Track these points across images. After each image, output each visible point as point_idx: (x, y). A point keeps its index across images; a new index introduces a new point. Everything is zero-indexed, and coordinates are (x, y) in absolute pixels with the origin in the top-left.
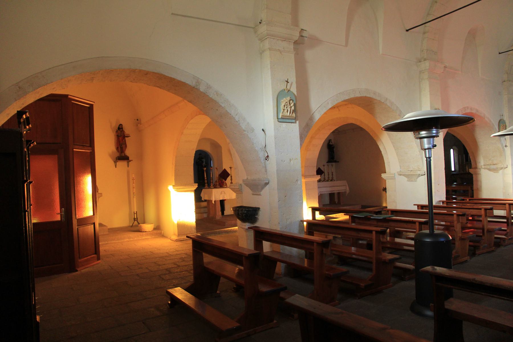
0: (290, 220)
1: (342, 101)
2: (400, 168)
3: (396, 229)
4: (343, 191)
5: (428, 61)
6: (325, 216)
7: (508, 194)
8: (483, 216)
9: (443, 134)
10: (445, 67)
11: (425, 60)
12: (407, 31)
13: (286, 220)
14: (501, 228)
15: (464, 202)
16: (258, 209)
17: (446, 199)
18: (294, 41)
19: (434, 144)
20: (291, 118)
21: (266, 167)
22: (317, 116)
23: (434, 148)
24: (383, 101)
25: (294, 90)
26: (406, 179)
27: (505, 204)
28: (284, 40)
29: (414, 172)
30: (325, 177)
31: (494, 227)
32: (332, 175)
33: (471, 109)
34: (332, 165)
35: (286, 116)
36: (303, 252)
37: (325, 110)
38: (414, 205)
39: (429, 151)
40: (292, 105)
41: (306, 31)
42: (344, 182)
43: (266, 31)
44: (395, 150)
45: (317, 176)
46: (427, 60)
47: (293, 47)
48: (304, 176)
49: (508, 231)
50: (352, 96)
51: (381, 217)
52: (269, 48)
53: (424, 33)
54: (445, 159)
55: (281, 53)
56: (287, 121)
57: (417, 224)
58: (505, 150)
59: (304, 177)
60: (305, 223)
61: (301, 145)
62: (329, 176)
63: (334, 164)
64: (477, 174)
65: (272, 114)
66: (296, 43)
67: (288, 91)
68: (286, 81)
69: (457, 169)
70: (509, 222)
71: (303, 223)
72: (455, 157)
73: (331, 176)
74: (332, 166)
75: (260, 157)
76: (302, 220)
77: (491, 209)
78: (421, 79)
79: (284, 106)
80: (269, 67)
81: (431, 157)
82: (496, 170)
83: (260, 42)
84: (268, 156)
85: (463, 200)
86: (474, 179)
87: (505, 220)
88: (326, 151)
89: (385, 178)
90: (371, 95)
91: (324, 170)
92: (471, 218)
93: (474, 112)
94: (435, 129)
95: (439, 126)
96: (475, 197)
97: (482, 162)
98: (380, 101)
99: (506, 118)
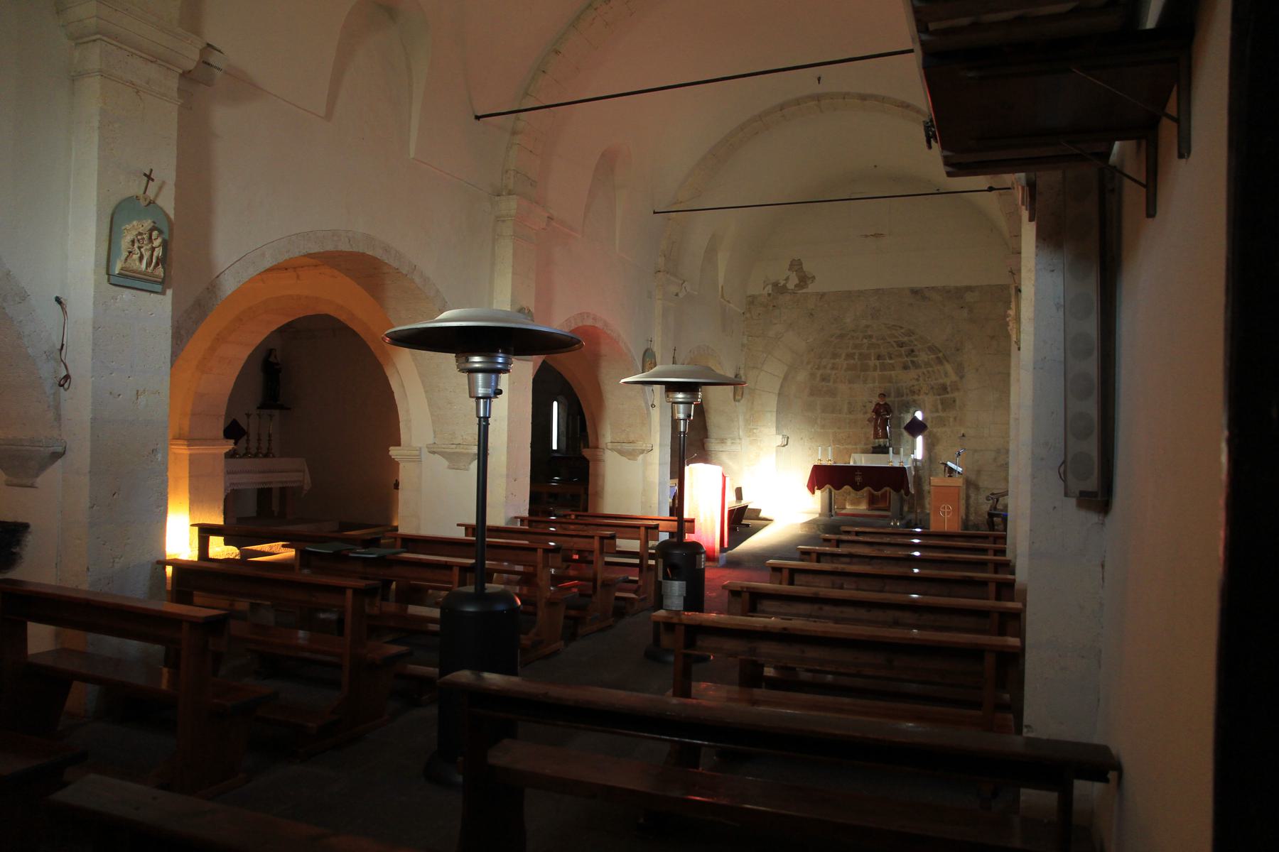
0: (122, 559)
1: (301, 254)
2: (433, 436)
3: (412, 582)
4: (294, 485)
5: (514, 196)
6: (239, 549)
7: (651, 507)
8: (597, 552)
9: (534, 366)
10: (550, 218)
11: (510, 193)
12: (478, 118)
13: (112, 560)
14: (628, 578)
15: (564, 520)
16: (24, 527)
17: (529, 514)
18: (181, 71)
19: (499, 388)
20: (149, 278)
21: (57, 407)
22: (229, 285)
23: (498, 396)
24: (404, 272)
25: (167, 202)
26: (445, 463)
27: (638, 527)
28: (150, 58)
29: (463, 448)
31: (613, 576)
33: (594, 319)
34: (271, 416)
35: (134, 272)
36: (157, 649)
37: (252, 272)
38: (458, 525)
39: (485, 404)
40: (156, 243)
41: (219, 51)
43: (95, 19)
44: (426, 392)
45: (224, 441)
46: (514, 194)
47: (177, 85)
48: (188, 440)
49: (641, 583)
50: (330, 247)
51: (373, 554)
52: (100, 71)
53: (514, 133)
54: (532, 423)
55: (137, 92)
56: (136, 286)
57: (456, 571)
58: (650, 413)
60: (169, 570)
61: (175, 355)
62: (259, 444)
63: (276, 413)
64: (598, 460)
65: (92, 259)
66: (185, 75)
67: (150, 203)
68: (145, 175)
69: (564, 446)
70: (644, 566)
71: (165, 568)
72: (561, 421)
74: (271, 420)
75: (40, 377)
76: (161, 558)
77: (613, 537)
78: (498, 235)
79: (133, 242)
80: (96, 124)
81: (489, 417)
82: (632, 455)
83: (73, 44)
84: (67, 377)
85: (565, 516)
86: (591, 471)
87: (637, 561)
89: (397, 458)
90: (378, 253)
91: (248, 425)
92: (576, 557)
93: (599, 325)
94: (502, 353)
95: (512, 349)
96: (590, 511)
97: (608, 435)
98: (397, 271)
99: (657, 349)
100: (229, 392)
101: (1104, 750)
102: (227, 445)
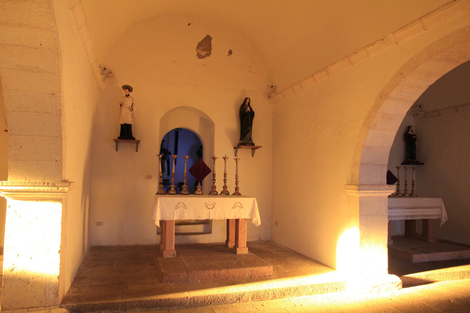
30: (400, 188)
32: (413, 185)
42: (438, 202)
45: (388, 186)
48: (359, 186)
59: (357, 188)
62: (406, 187)
73: (409, 188)
88: (402, 144)
100: (391, 146)
101: (254, 144)
102: (390, 190)
